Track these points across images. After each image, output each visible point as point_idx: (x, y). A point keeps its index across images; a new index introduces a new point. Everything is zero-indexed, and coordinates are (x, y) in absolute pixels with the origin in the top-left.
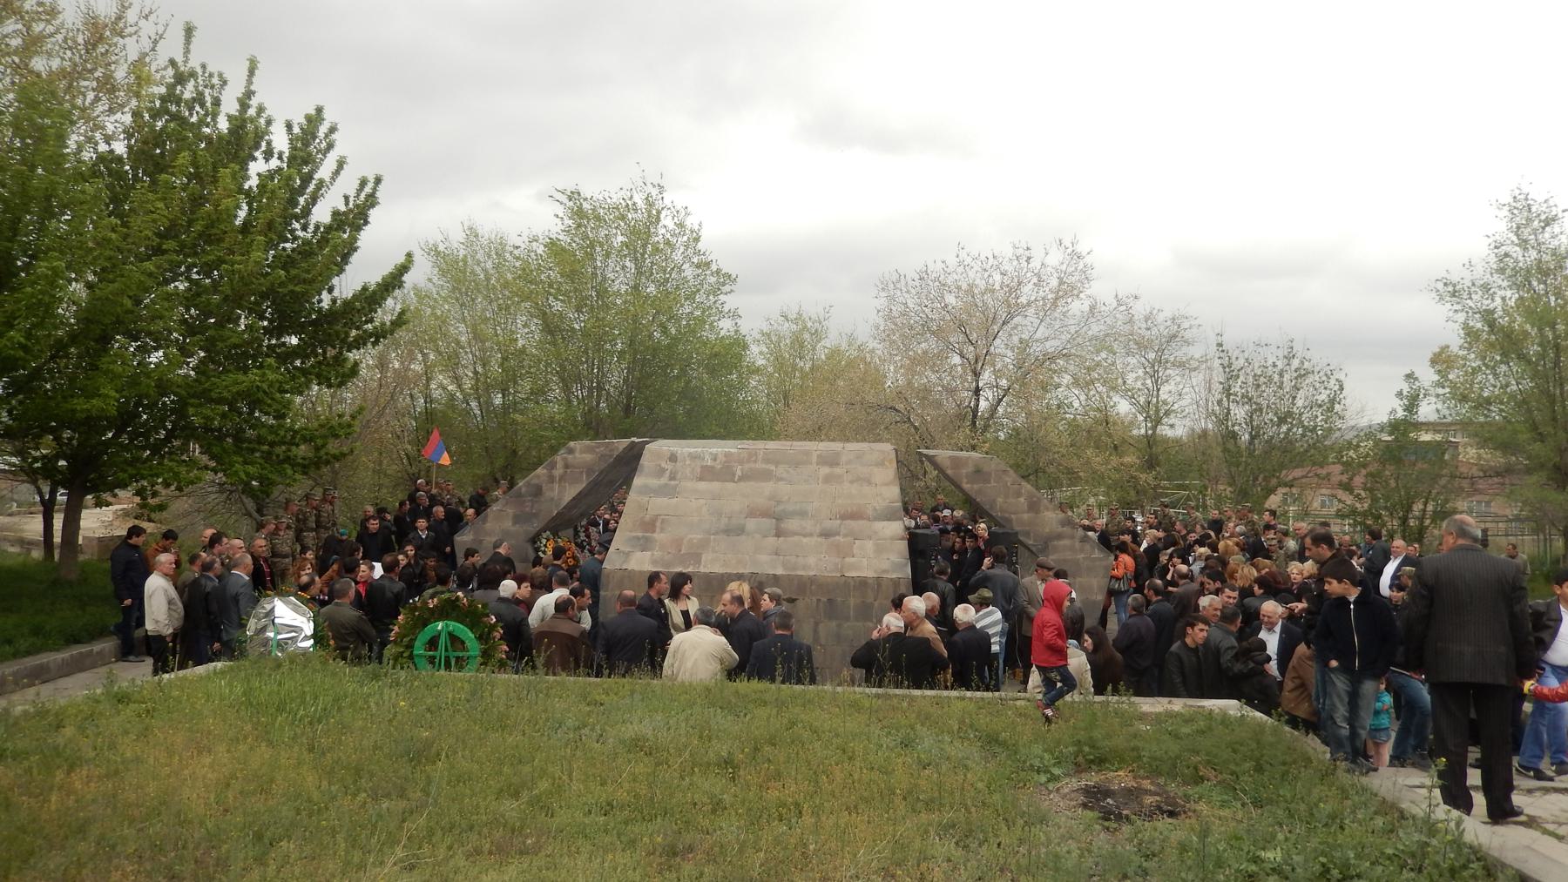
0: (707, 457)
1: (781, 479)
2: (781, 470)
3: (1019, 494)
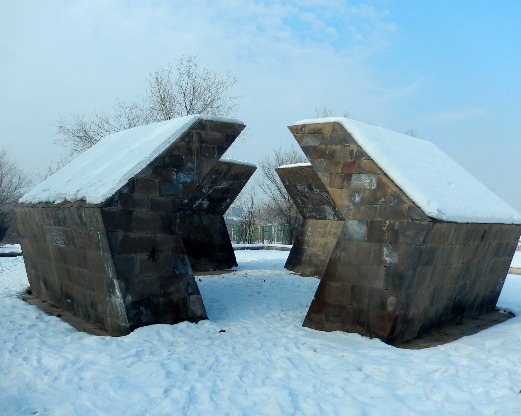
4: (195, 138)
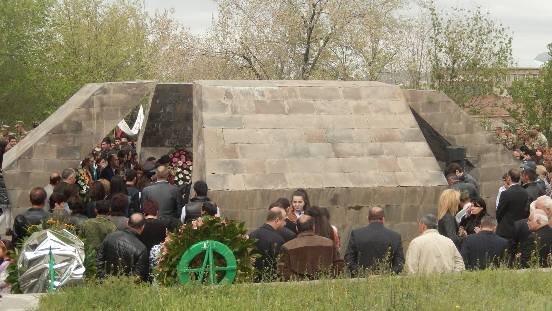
0: (256, 94)
1: (321, 111)
2: (318, 103)
3: (459, 120)
4: (96, 103)
